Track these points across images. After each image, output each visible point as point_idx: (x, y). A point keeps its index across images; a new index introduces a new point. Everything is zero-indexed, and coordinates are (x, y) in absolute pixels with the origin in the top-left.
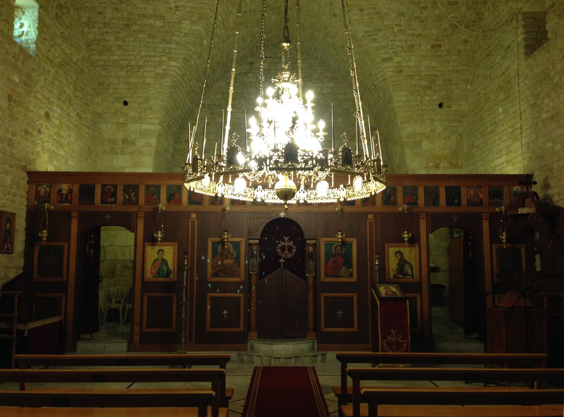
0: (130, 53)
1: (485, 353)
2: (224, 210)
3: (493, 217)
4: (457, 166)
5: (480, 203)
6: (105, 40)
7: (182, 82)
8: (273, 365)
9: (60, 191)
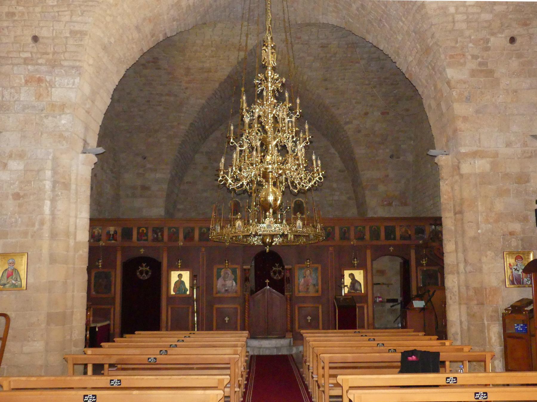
5: (410, 237)
9: (109, 232)
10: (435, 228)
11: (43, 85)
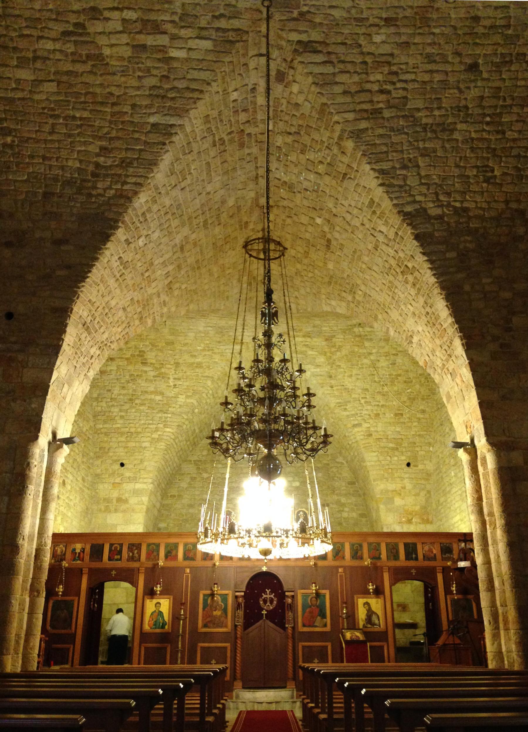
0: (131, 421)
1: (396, 662)
2: (215, 565)
3: (445, 570)
4: (428, 522)
5: (434, 558)
6: (110, 411)
7: (174, 443)
8: (256, 709)
10: (465, 545)
11: (13, 365)
